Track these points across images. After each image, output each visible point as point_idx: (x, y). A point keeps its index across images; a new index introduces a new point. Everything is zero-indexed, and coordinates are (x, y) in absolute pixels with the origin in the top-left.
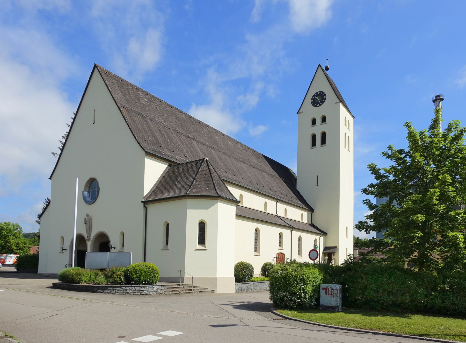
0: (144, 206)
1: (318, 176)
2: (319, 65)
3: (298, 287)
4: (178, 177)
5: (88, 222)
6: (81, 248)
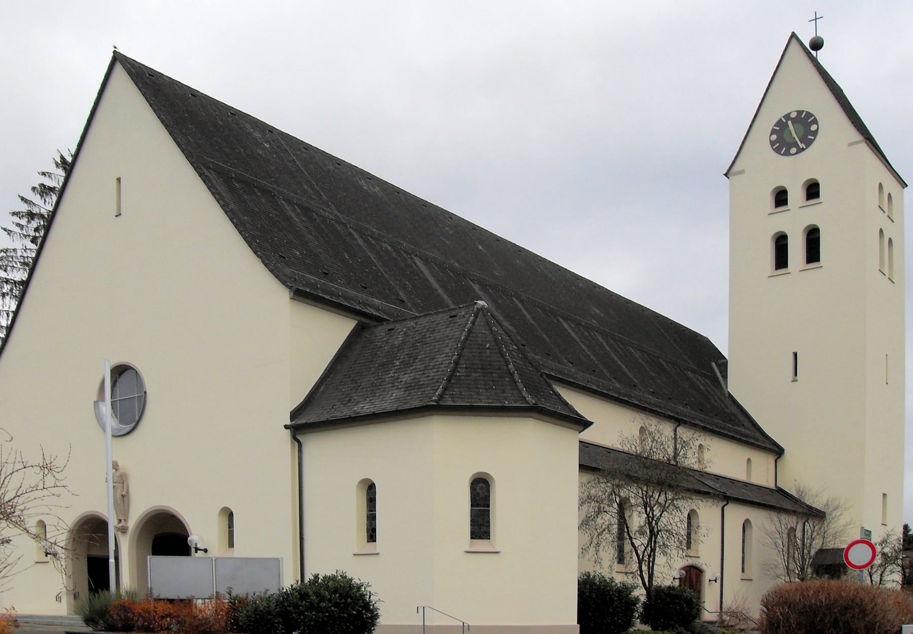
0: (294, 438)
1: (795, 355)
2: (793, 35)
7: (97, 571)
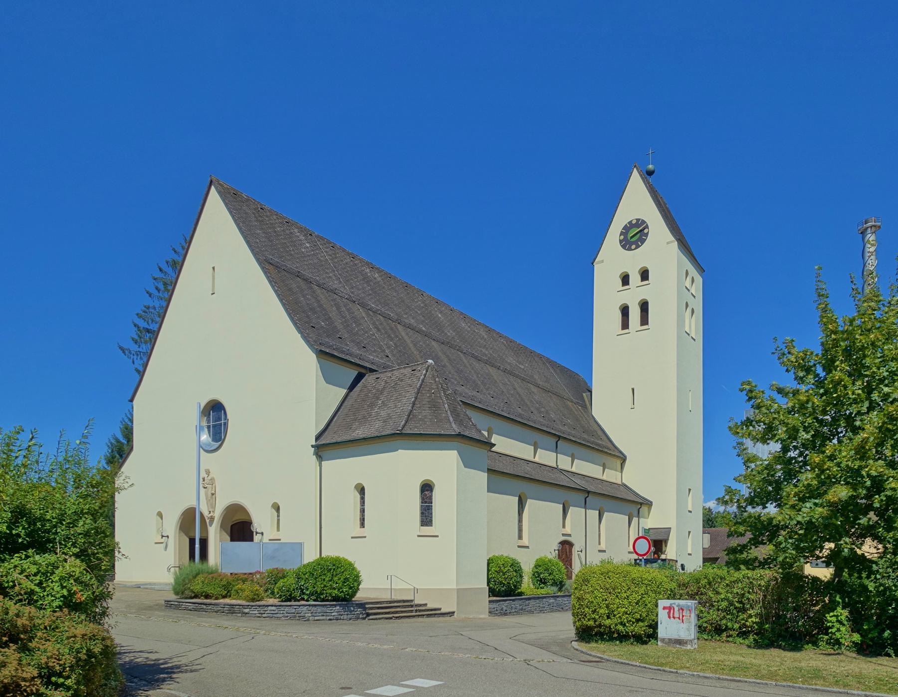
3: (57, 588)
4: (378, 399)
5: (206, 483)
6: (204, 535)
7: (198, 548)
